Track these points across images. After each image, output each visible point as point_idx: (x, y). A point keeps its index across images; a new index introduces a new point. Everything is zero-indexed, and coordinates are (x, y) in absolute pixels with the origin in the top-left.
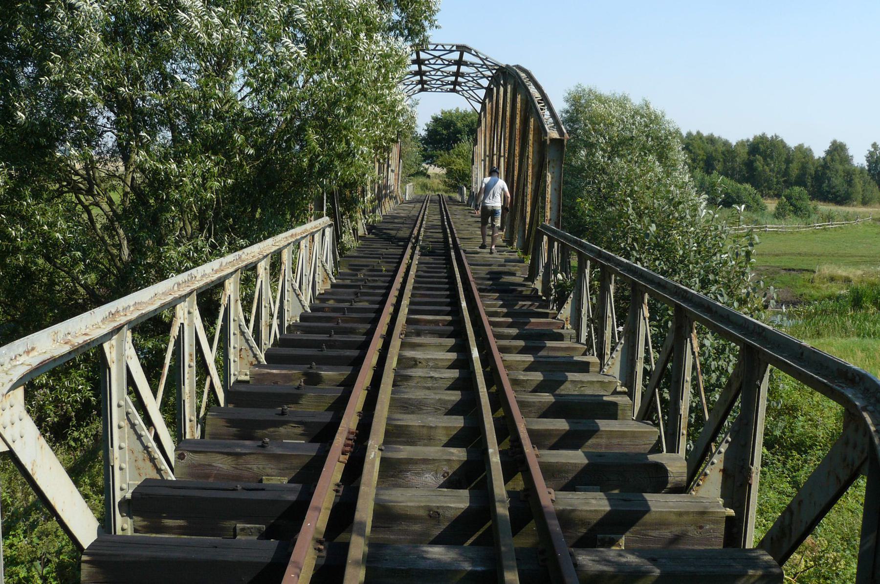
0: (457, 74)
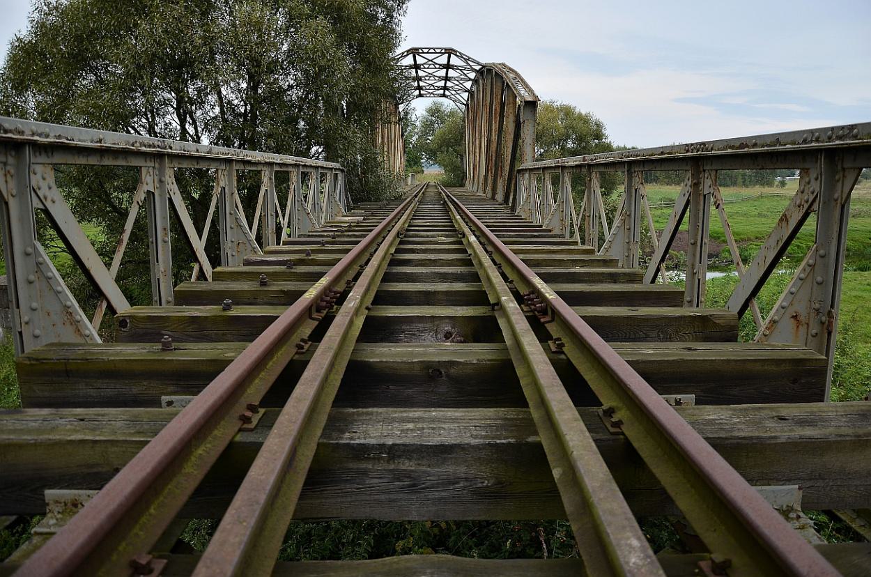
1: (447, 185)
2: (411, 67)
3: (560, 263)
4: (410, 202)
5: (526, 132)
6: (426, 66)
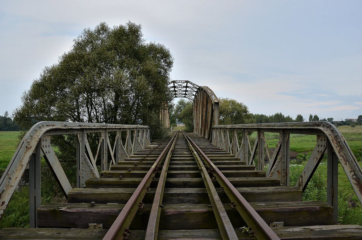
0: (186, 91)
1: (186, 131)
2: (173, 87)
3: (222, 160)
4: (174, 140)
5: (215, 113)
6: (178, 87)
